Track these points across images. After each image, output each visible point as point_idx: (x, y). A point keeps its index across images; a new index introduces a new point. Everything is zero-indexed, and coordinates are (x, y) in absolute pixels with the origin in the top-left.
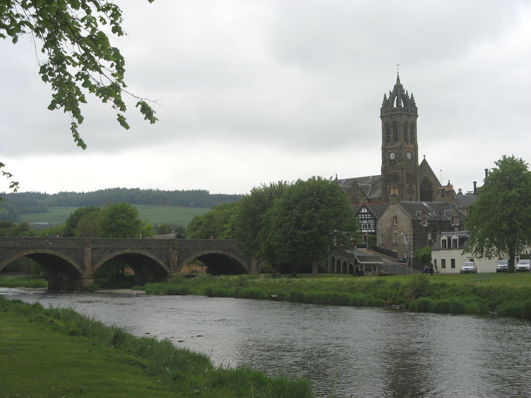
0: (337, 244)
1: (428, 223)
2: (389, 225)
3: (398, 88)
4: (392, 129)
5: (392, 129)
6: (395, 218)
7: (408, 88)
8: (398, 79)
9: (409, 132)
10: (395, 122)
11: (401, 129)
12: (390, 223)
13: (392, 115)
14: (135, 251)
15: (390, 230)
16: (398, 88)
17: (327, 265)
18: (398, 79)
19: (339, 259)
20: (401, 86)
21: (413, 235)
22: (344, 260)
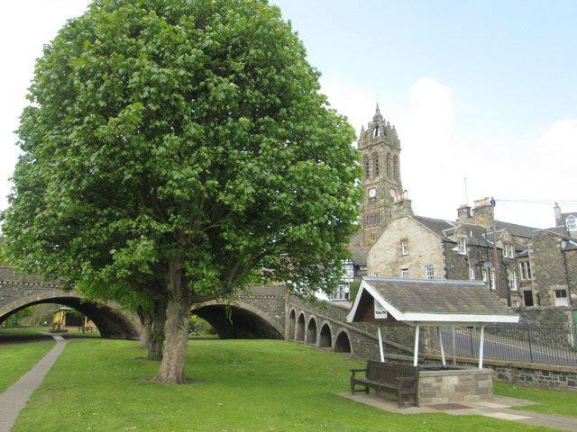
0: (228, 252)
1: (469, 249)
2: (391, 255)
3: (378, 118)
4: (371, 162)
5: (371, 162)
6: (405, 240)
7: (390, 118)
8: (377, 110)
9: (392, 166)
10: (375, 154)
11: (382, 161)
12: (394, 252)
13: (372, 146)
14: (259, 312)
15: (394, 265)
16: (378, 118)
17: (283, 326)
18: (377, 110)
19: (302, 315)
20: (381, 116)
21: (446, 269)
22: (312, 316)
